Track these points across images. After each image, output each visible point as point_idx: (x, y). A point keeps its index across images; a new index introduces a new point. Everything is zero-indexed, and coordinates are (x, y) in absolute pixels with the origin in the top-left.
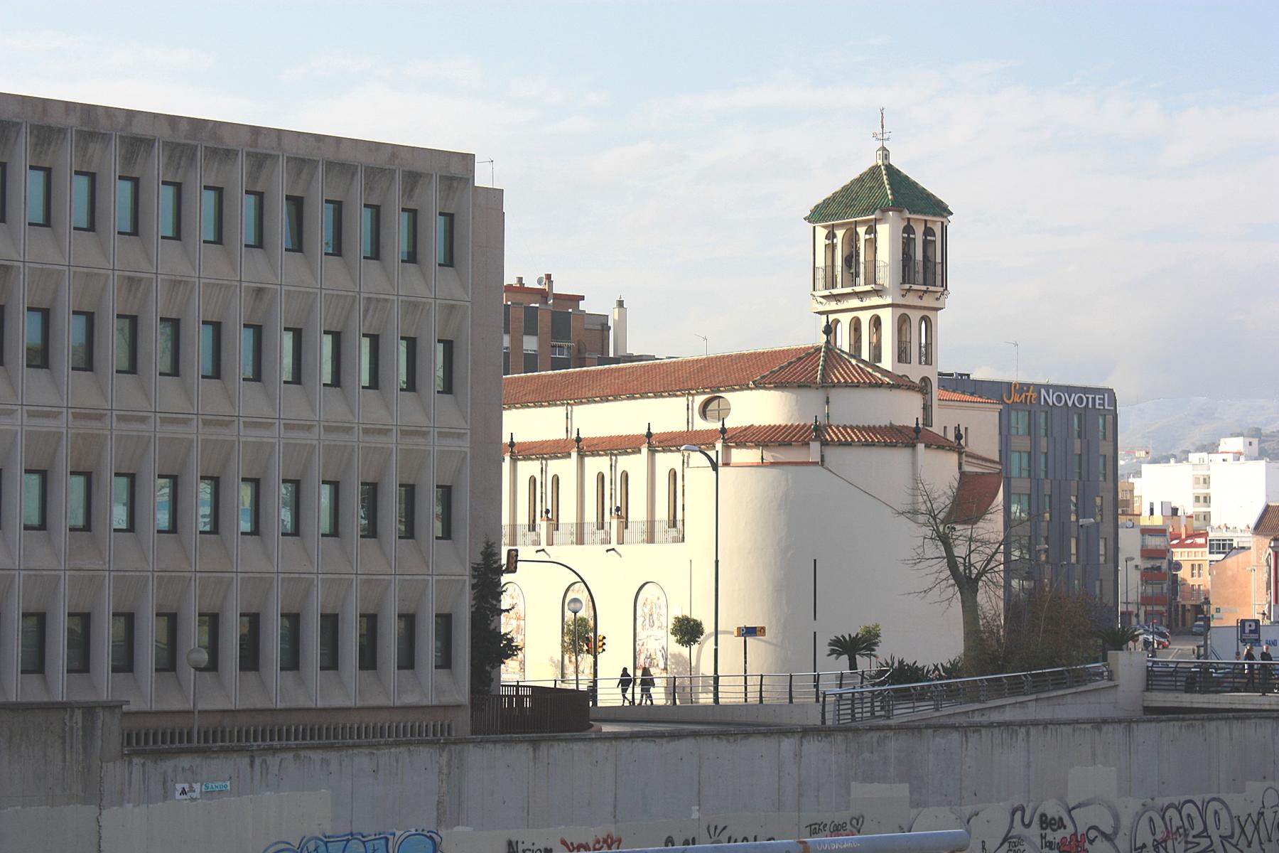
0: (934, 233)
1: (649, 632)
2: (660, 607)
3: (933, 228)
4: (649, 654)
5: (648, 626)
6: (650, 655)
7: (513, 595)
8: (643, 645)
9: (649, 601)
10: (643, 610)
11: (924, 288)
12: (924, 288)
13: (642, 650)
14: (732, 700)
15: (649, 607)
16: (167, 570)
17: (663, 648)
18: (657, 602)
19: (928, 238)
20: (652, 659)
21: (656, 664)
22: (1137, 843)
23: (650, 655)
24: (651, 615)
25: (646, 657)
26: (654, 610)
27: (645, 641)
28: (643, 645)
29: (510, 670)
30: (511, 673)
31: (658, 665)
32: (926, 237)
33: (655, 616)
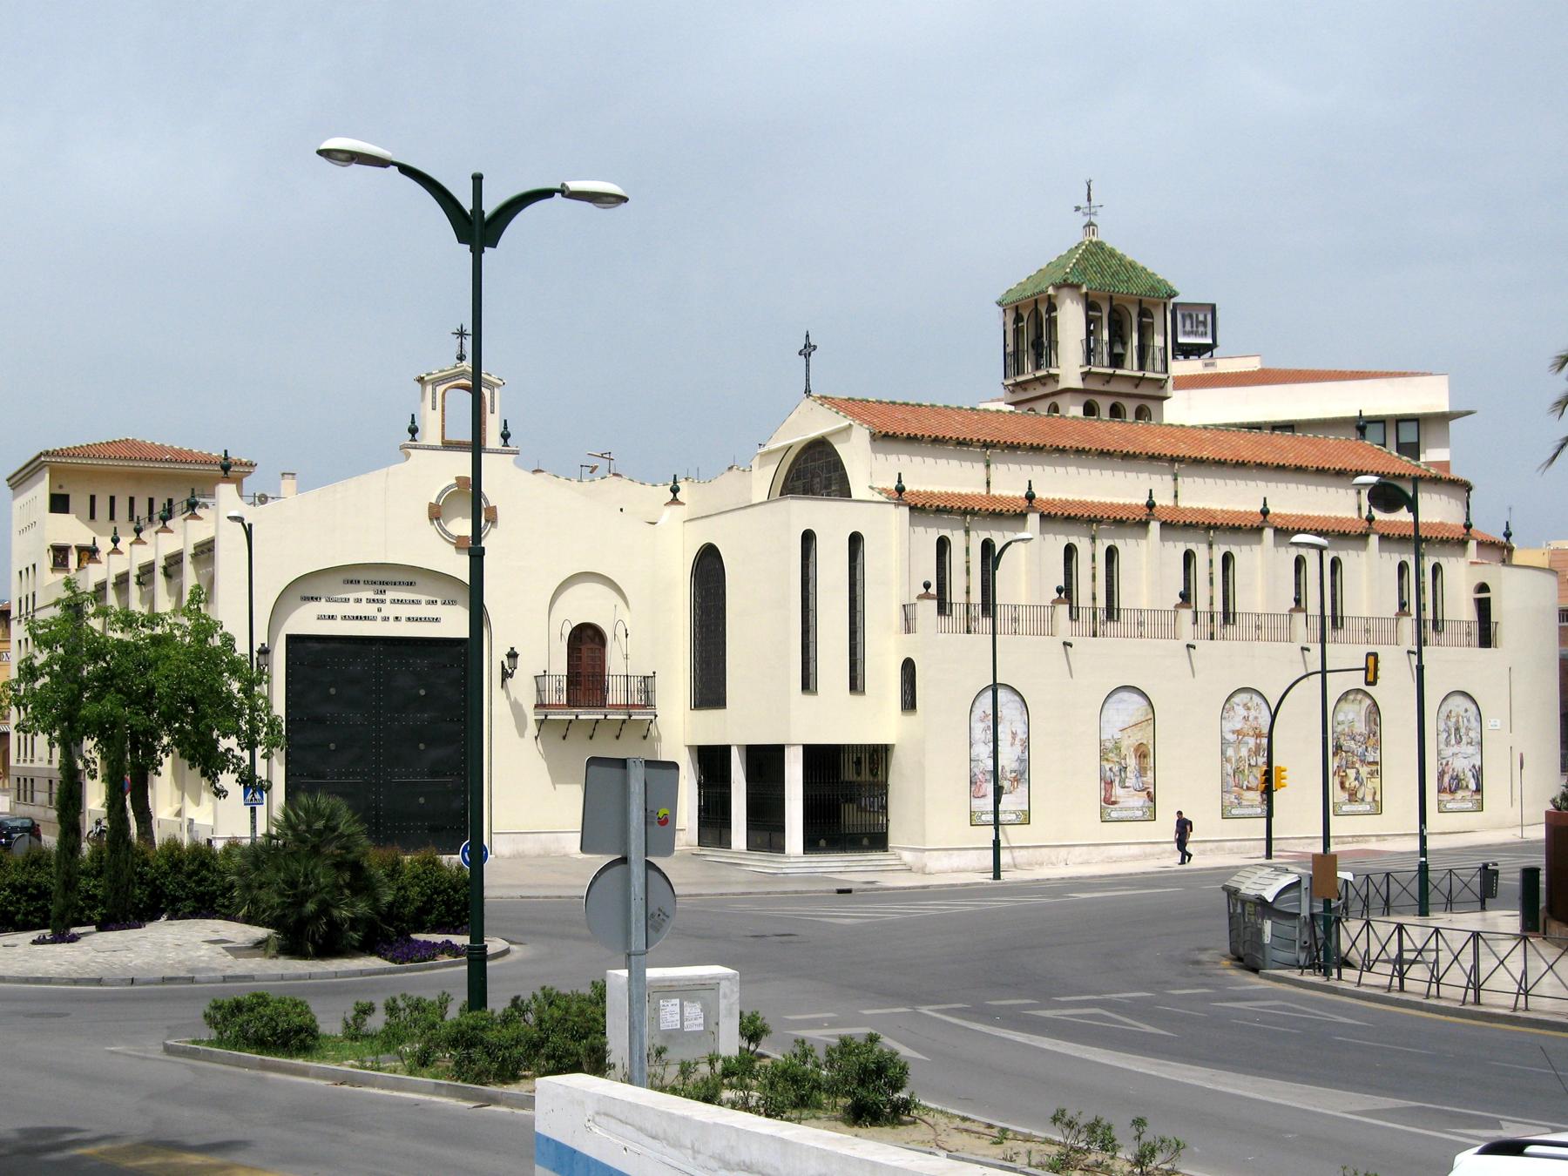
0: (1152, 314)
1: (1456, 749)
2: (1468, 720)
3: (1152, 310)
4: (1455, 774)
5: (1453, 742)
6: (1457, 775)
7: (1249, 705)
8: (1447, 764)
9: (1453, 714)
10: (1446, 724)
11: (1110, 371)
12: (1110, 371)
13: (1446, 770)
14: (869, 857)
15: (1453, 720)
16: (1308, 665)
17: (1474, 767)
18: (1464, 715)
19: (1144, 320)
20: (1460, 781)
21: (1465, 785)
22: (1515, 976)
23: (1457, 775)
24: (1457, 729)
25: (1452, 778)
26: (1461, 723)
27: (1451, 760)
28: (1447, 764)
29: (1244, 803)
30: (1248, 806)
31: (1467, 786)
32: (1141, 320)
33: (1463, 731)
